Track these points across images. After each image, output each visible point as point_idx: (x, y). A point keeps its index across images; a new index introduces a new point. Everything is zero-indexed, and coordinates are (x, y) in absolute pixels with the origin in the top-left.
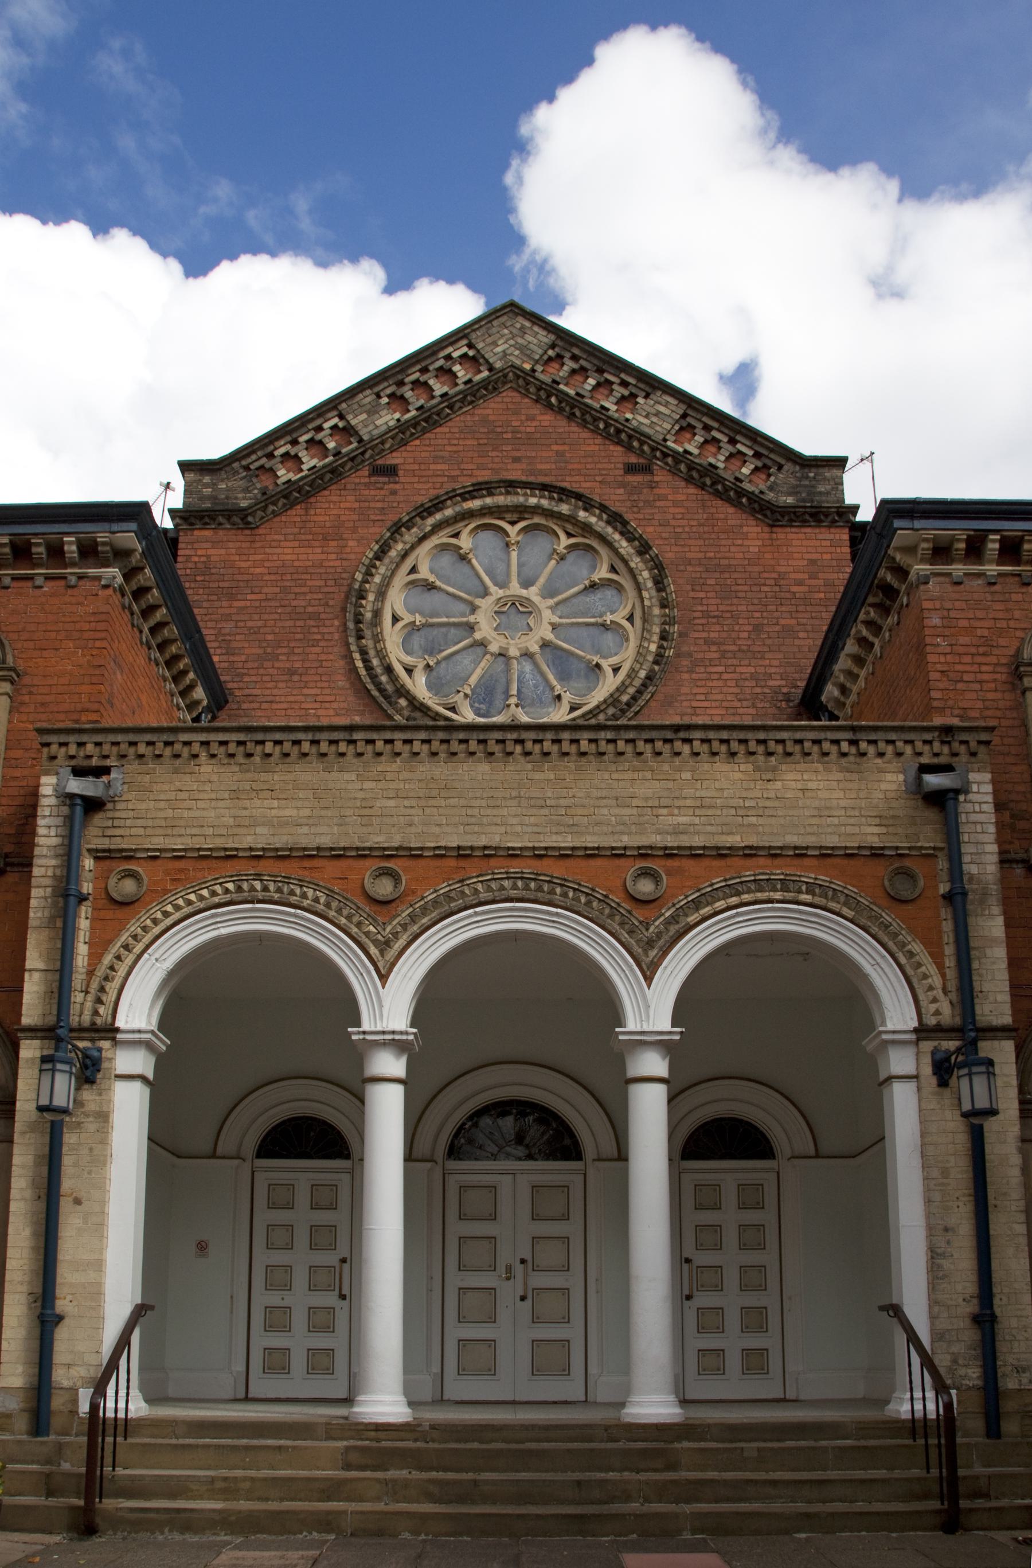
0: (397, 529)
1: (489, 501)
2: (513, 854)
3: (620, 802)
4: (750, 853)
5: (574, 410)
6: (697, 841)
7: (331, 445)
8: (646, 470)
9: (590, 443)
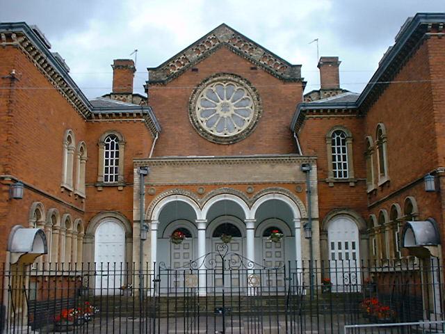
1: (219, 78)
4: (270, 183)
6: (260, 181)
7: (182, 63)
8: (255, 68)
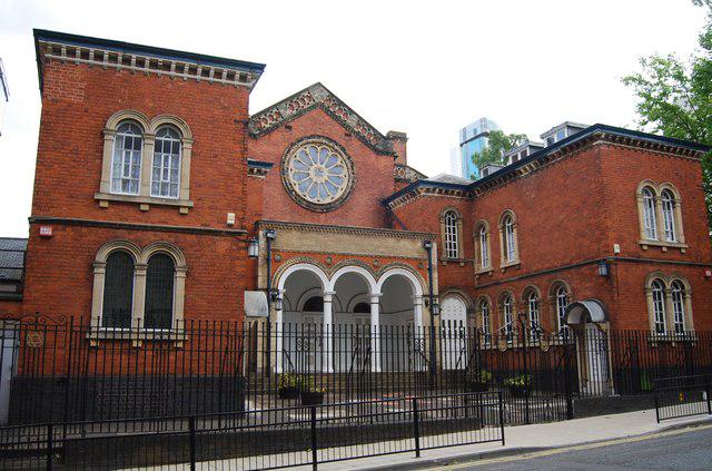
0: (292, 145)
2: (353, 256)
3: (373, 246)
5: (333, 116)
9: (338, 127)
